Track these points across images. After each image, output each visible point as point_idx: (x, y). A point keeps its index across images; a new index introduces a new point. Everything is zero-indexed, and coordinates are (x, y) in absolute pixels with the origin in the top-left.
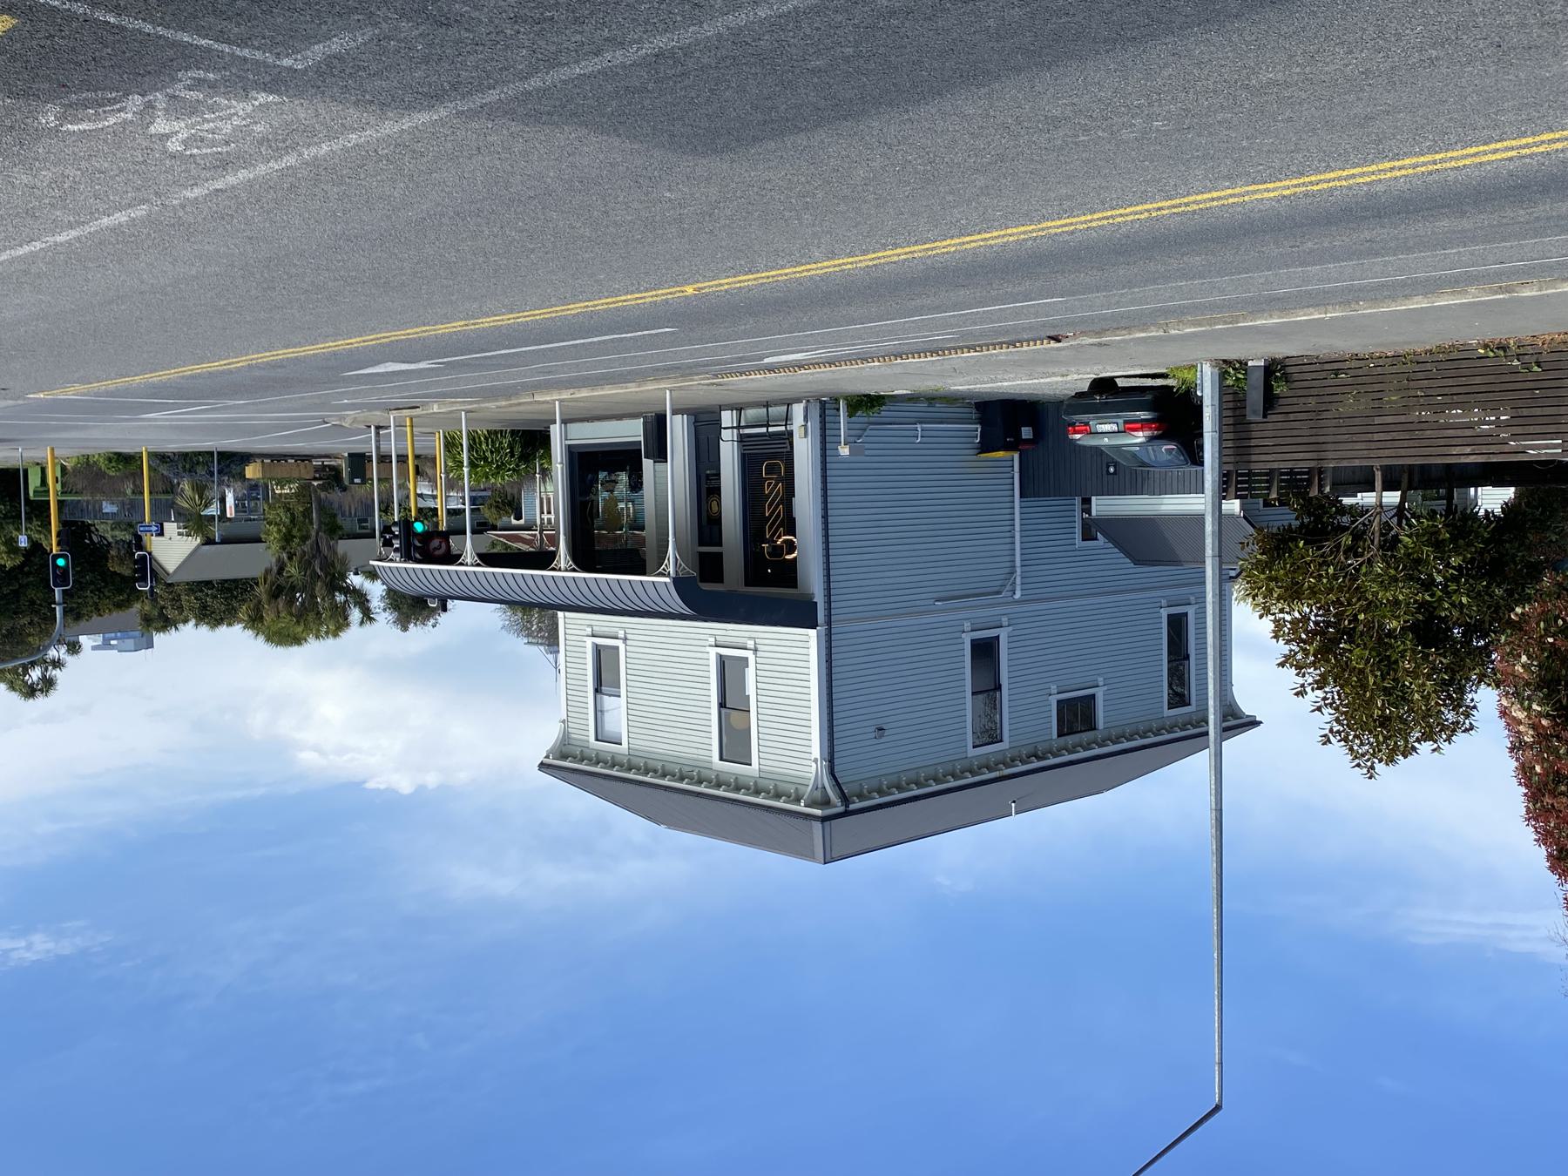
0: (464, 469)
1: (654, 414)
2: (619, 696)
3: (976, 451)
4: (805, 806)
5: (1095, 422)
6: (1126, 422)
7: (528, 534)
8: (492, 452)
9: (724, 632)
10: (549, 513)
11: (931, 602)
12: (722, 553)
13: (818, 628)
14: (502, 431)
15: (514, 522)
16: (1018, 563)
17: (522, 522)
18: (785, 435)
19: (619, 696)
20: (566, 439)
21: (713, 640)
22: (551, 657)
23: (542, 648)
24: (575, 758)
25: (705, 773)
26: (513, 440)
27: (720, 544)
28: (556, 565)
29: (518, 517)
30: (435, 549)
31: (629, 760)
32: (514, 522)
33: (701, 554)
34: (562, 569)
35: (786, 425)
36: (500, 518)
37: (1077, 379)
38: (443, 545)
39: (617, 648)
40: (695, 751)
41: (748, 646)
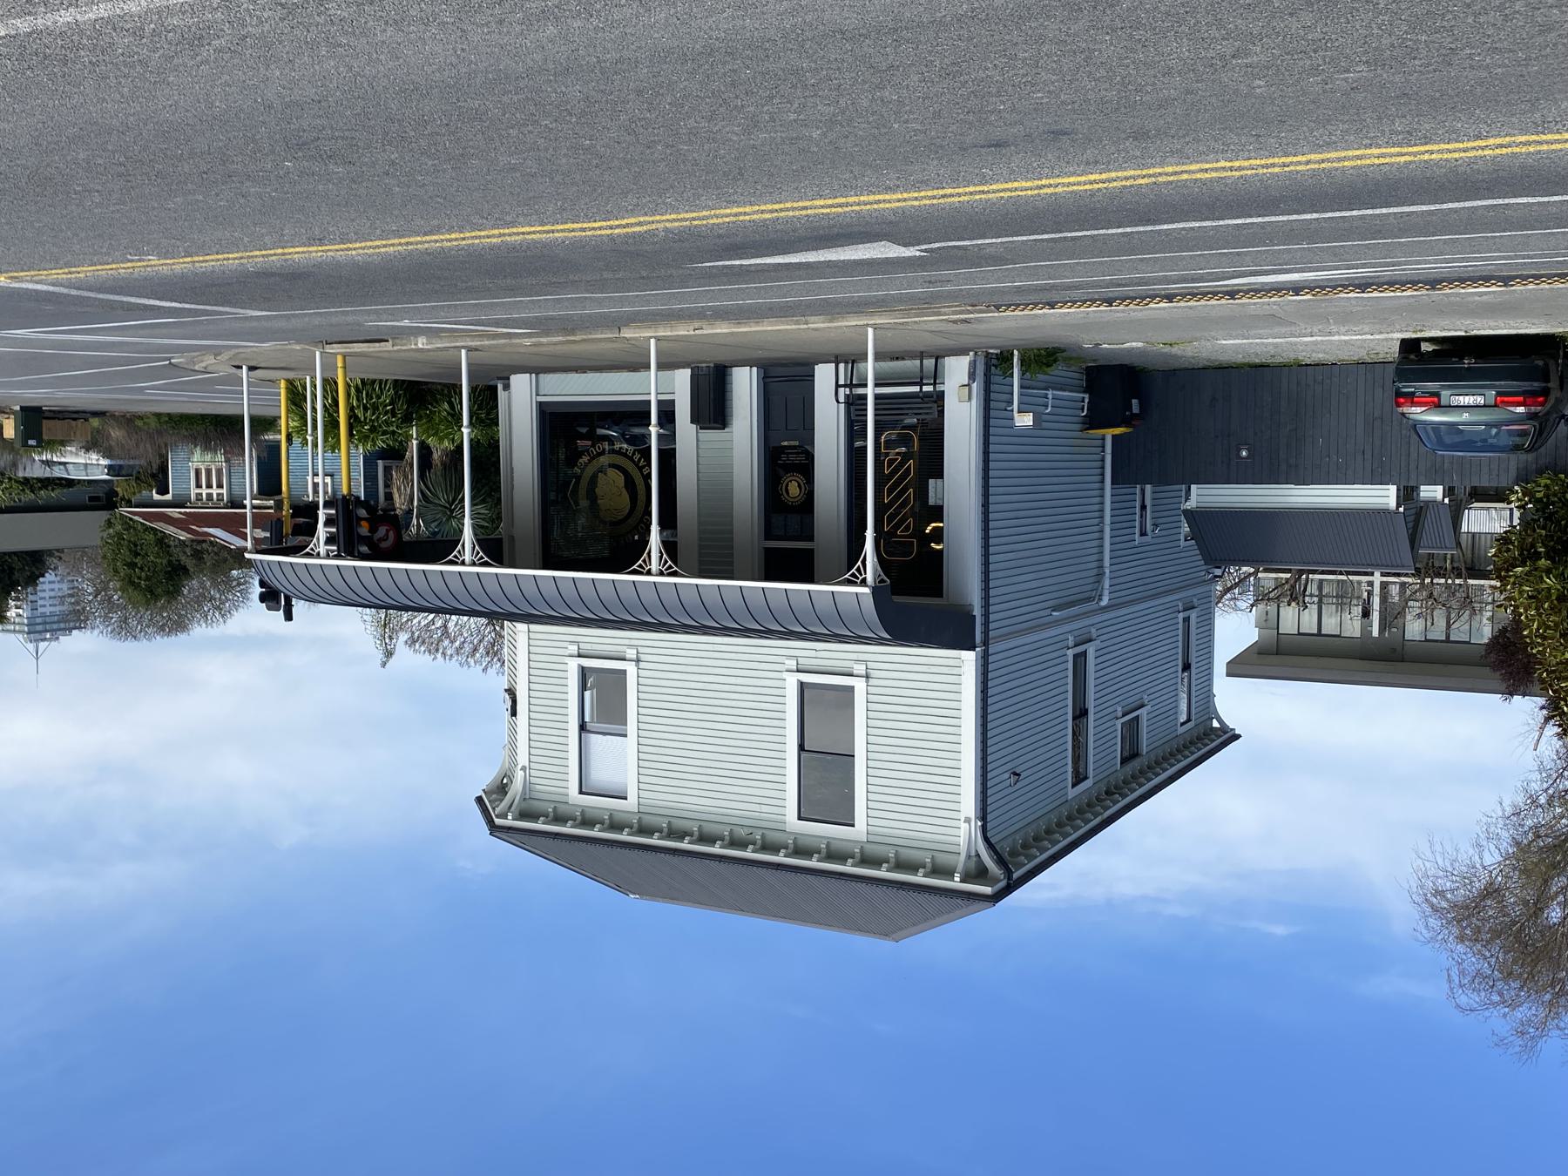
0: (463, 429)
1: (712, 365)
2: (625, 736)
3: (1078, 427)
4: (513, 820)
5: (1449, 392)
6: (1499, 394)
7: (180, 513)
8: (366, 409)
9: (813, 653)
10: (220, 486)
11: (1048, 611)
12: (813, 550)
13: (977, 649)
14: (381, 381)
15: (157, 497)
16: (1107, 562)
17: (169, 497)
18: (932, 397)
19: (625, 736)
20: (537, 395)
21: (576, 648)
22: (31, 646)
23: (20, 636)
24: (575, 820)
25: (562, 808)
26: (396, 393)
27: (811, 538)
28: (640, 566)
29: (163, 491)
30: (381, 540)
31: (640, 820)
32: (157, 497)
33: (767, 550)
34: (467, 561)
35: (935, 384)
36: (140, 492)
37: (1384, 342)
38: (391, 534)
39: (624, 672)
40: (756, 808)
41: (628, 656)
